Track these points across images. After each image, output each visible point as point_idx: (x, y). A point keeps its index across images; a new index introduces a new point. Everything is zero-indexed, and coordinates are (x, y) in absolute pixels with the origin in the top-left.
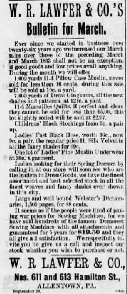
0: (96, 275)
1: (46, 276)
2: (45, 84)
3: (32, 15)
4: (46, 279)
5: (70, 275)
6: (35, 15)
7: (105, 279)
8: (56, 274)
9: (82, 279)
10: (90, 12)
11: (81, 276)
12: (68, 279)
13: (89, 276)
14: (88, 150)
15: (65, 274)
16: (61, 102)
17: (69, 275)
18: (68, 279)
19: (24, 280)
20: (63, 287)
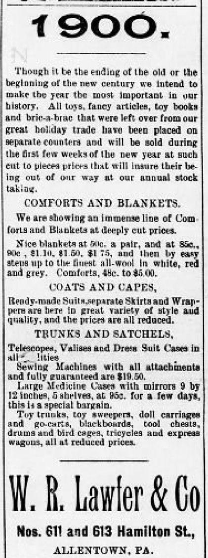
0: (154, 529)
1: (70, 530)
2: (68, 83)
3: (59, 508)
4: (70, 534)
5: (110, 528)
6: (64, 508)
7: (169, 535)
8: (87, 527)
9: (131, 535)
10: (161, 501)
11: (128, 530)
12: (106, 534)
13: (142, 530)
14: (145, 214)
15: (102, 528)
16: (103, 436)
17: (108, 529)
18: (106, 534)
19: (33, 536)
20: (97, 553)
